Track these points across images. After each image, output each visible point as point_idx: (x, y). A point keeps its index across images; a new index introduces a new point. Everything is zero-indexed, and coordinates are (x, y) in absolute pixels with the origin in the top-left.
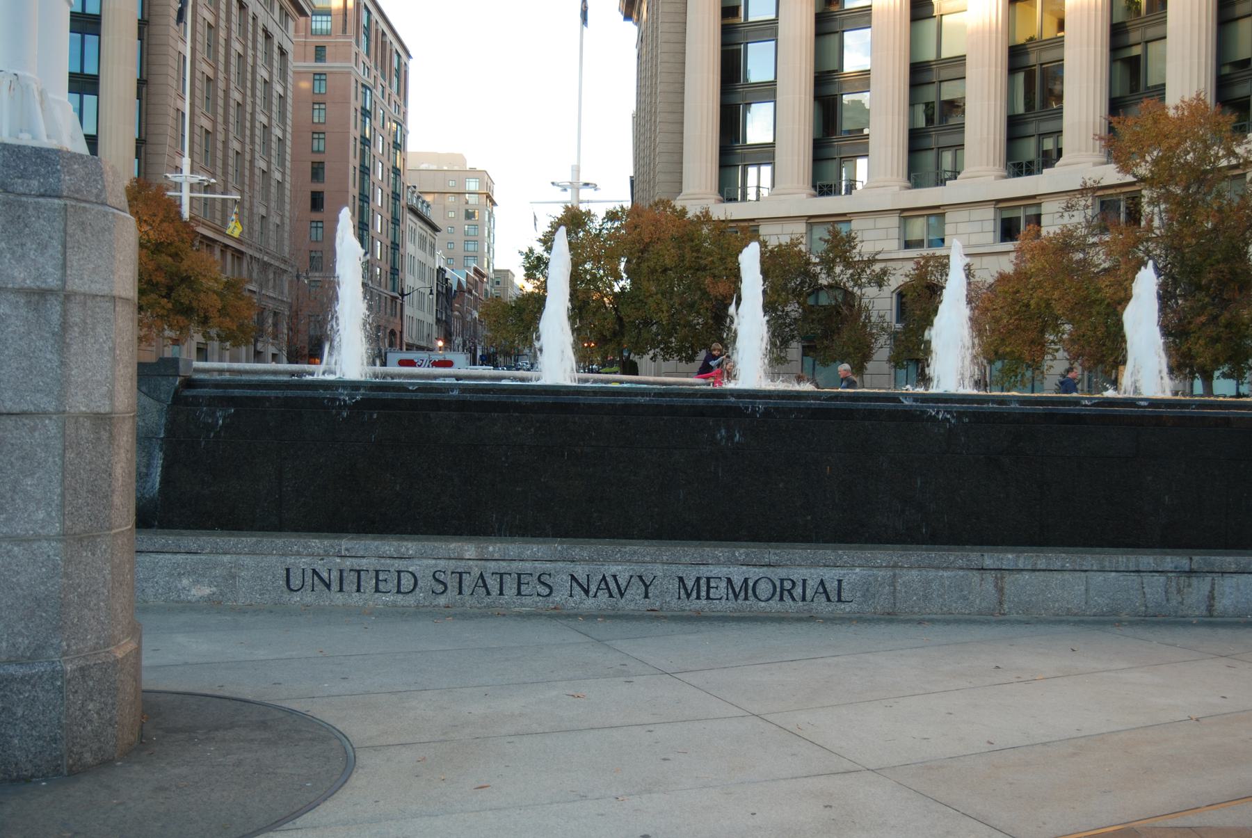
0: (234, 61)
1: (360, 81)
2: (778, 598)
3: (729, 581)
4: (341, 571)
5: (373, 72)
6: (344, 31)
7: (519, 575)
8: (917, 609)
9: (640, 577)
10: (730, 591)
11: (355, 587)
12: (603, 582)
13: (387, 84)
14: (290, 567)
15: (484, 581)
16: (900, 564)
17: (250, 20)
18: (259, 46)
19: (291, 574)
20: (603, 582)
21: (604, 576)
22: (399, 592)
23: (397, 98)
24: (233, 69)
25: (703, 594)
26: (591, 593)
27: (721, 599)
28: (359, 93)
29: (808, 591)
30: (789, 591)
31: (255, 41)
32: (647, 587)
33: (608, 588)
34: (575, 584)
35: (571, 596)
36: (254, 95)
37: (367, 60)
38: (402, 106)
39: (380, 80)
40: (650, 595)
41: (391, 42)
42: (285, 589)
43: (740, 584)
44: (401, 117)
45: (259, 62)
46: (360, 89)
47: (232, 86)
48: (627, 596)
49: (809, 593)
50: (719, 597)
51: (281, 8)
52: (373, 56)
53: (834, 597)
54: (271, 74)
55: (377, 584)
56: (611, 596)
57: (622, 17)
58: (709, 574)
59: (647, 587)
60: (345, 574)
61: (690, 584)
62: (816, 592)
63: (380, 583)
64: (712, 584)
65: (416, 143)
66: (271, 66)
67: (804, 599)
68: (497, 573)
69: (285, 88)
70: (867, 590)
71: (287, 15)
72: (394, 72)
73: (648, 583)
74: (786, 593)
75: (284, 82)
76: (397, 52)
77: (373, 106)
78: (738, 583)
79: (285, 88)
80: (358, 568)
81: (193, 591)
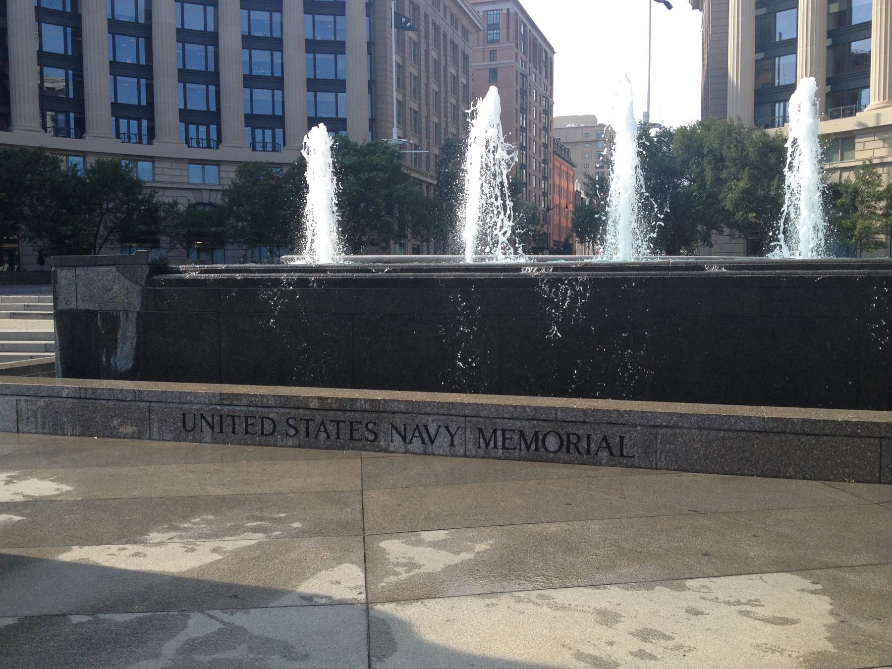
0: (431, 64)
1: (519, 71)
2: (565, 451)
3: (522, 434)
4: (221, 417)
5: (528, 65)
6: (508, 39)
7: (351, 423)
8: (699, 467)
9: (447, 428)
10: (522, 443)
11: (231, 429)
12: (417, 431)
13: (538, 72)
14: (186, 412)
15: (325, 427)
16: (680, 424)
17: (442, 37)
18: (449, 53)
19: (186, 418)
20: (417, 431)
21: (417, 426)
22: (262, 434)
23: (545, 81)
24: (431, 70)
25: (500, 444)
26: (407, 441)
27: (515, 448)
28: (519, 79)
29: (593, 445)
30: (575, 444)
31: (445, 50)
32: (452, 436)
33: (421, 436)
34: (394, 432)
35: (392, 441)
36: (446, 86)
37: (524, 57)
38: (550, 87)
39: (533, 69)
40: (455, 443)
41: (540, 44)
42: (182, 429)
43: (531, 436)
44: (549, 93)
45: (449, 63)
46: (519, 76)
47: (431, 80)
48: (437, 443)
49: (593, 446)
50: (514, 447)
51: (463, 27)
52: (528, 54)
53: (616, 451)
54: (457, 71)
55: (247, 426)
56: (423, 443)
57: (692, 7)
58: (505, 427)
59: (452, 436)
60: (224, 419)
61: (488, 435)
62: (600, 447)
63: (249, 426)
64: (507, 436)
65: (558, 111)
66: (457, 66)
67: (588, 452)
68: (334, 421)
69: (468, 80)
70: (648, 447)
71: (467, 32)
72: (542, 63)
73: (453, 433)
74: (572, 446)
75: (418, 66)
76: (545, 50)
77: (528, 87)
78: (529, 435)
79: (468, 80)
80: (233, 414)
81: (121, 430)
